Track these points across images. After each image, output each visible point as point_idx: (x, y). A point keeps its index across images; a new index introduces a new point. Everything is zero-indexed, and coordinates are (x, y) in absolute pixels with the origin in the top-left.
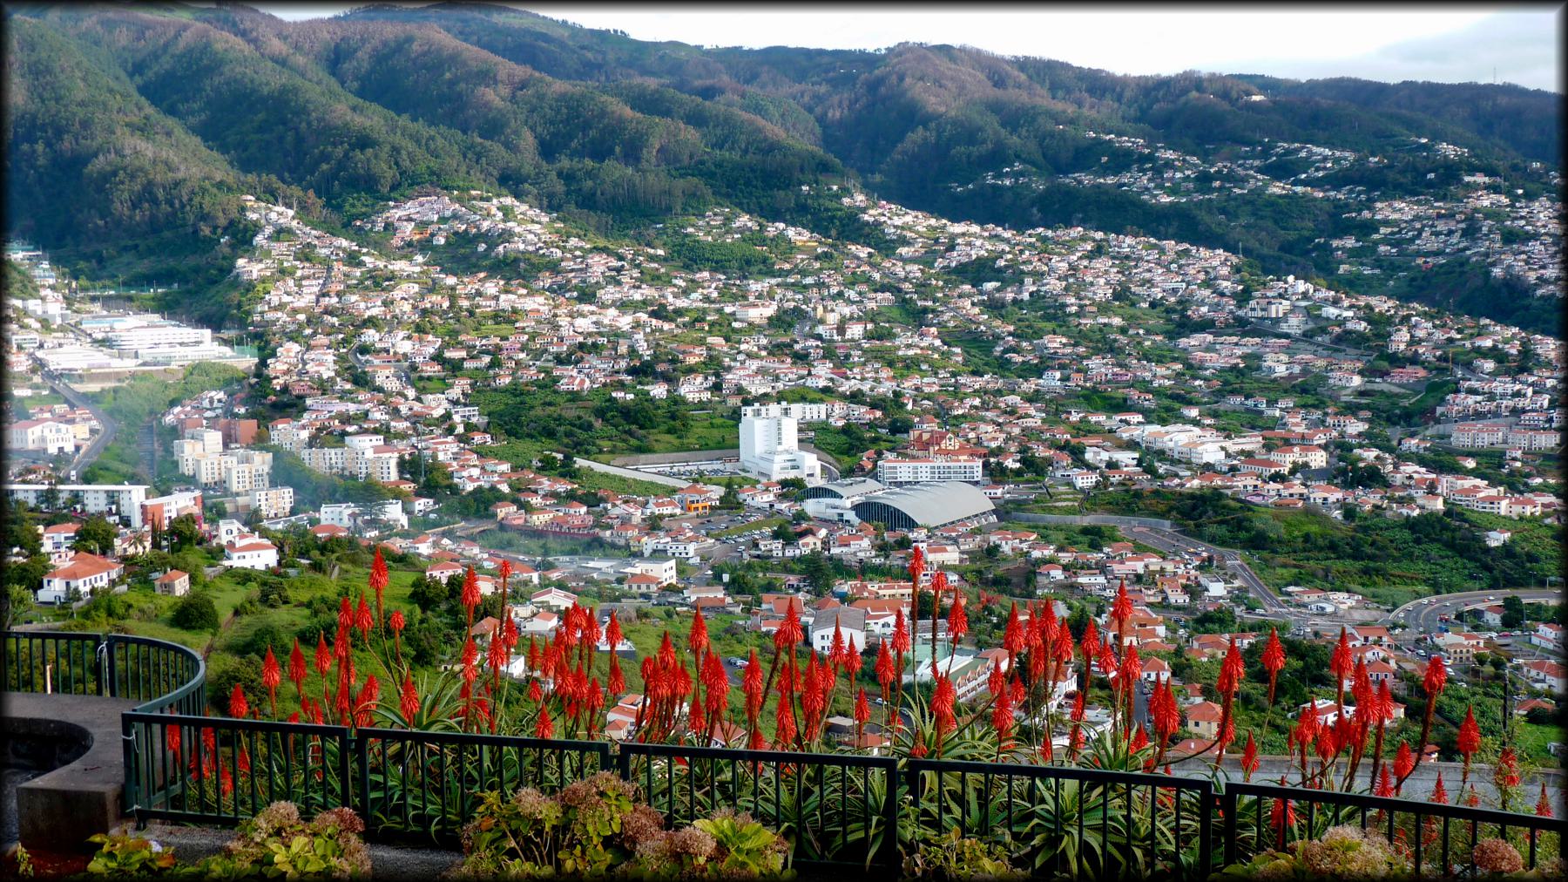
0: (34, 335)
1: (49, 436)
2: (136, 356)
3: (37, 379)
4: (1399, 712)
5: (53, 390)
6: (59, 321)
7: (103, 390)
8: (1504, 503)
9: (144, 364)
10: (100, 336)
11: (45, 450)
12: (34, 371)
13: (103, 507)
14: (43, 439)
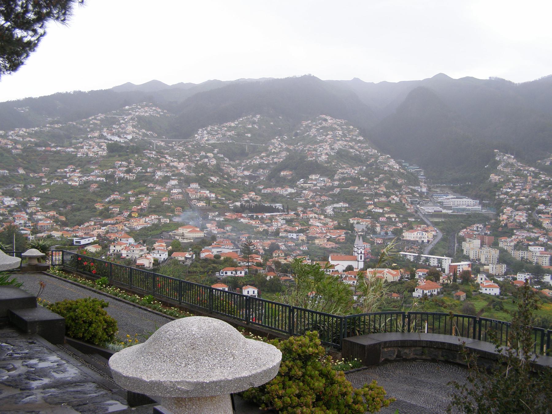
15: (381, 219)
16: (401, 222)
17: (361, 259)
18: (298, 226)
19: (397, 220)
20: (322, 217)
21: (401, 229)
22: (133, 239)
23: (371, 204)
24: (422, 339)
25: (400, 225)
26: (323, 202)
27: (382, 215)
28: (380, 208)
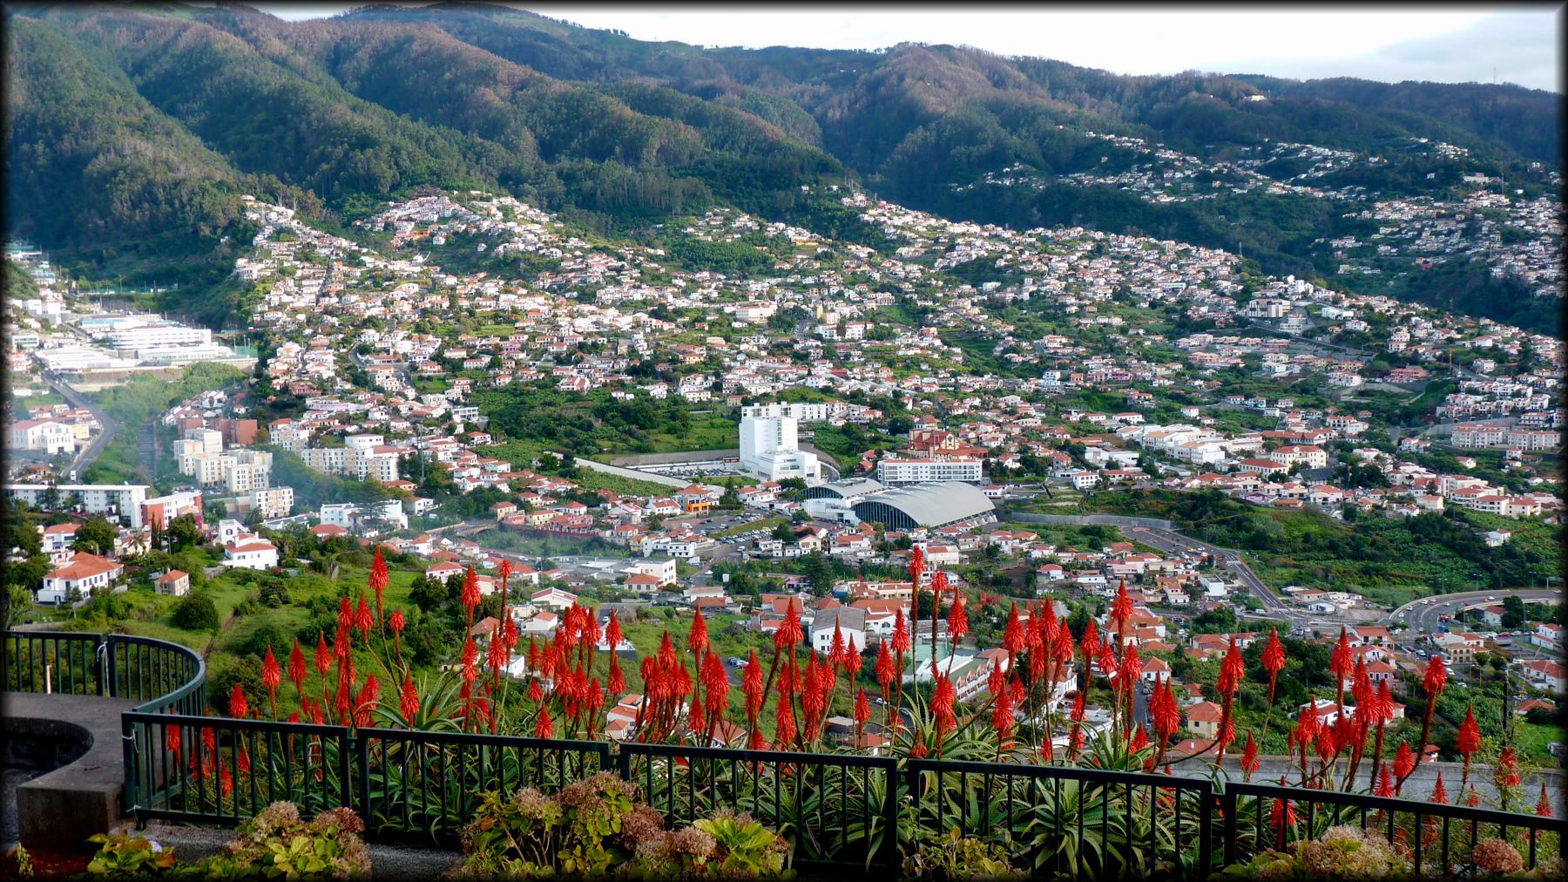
0: (34, 335)
1: (49, 436)
2: (136, 356)
3: (37, 379)
4: (1399, 712)
5: (53, 390)
6: (59, 321)
7: (103, 390)
8: (1504, 503)
9: (144, 364)
10: (100, 336)
11: (45, 450)
12: (34, 371)
13: (103, 507)
14: (43, 439)
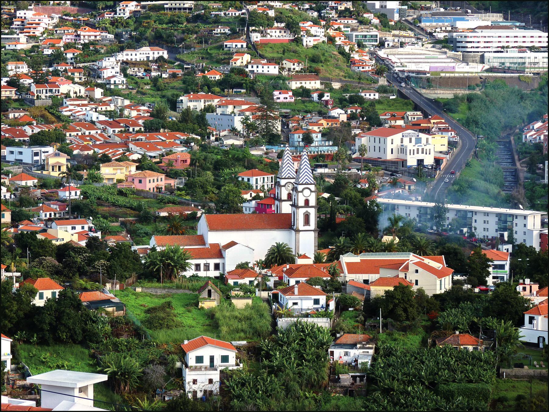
0: (374, 32)
1: (410, 146)
2: (482, 60)
3: (383, 81)
4: (446, 371)
5: (401, 94)
6: (396, 17)
7: (456, 97)
8: (148, 87)
9: (491, 70)
10: (441, 36)
11: (404, 162)
12: (379, 72)
13: (492, 233)
14: (402, 150)
15: (280, 97)
16: (342, 103)
17: (307, 222)
18: (30, 124)
19: (327, 97)
20: (98, 93)
21: (346, 126)
22: (334, 87)
23: (240, 53)
24: (219, 380)
25: (340, 114)
26: (85, 46)
27: (278, 82)
28: (271, 61)
